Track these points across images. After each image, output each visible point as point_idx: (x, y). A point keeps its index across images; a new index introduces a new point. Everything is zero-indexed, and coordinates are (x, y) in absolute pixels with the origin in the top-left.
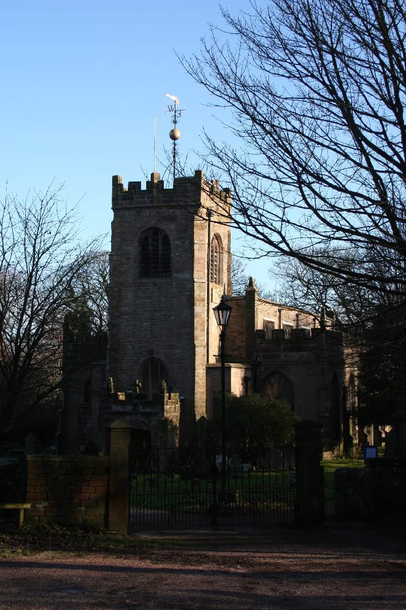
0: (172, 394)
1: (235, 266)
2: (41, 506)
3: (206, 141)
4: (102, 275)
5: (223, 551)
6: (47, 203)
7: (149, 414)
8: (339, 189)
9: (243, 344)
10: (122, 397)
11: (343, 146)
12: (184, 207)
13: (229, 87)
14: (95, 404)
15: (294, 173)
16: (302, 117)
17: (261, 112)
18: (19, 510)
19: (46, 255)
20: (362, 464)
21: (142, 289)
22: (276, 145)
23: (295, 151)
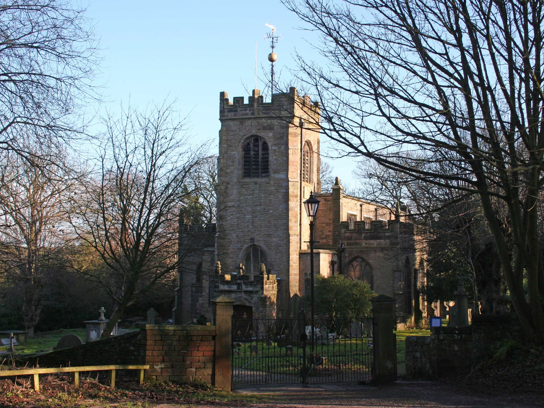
0: (270, 276)
1: (324, 169)
2: (158, 367)
3: (297, 58)
4: (212, 176)
5: (310, 404)
6: (164, 113)
7: (251, 292)
8: (409, 101)
9: (330, 234)
10: (228, 277)
11: (412, 64)
12: (281, 118)
13: (316, 15)
14: (206, 284)
15: (371, 87)
16: (377, 40)
17: (343, 36)
18: (139, 371)
19: (162, 157)
20: (428, 333)
21: (244, 187)
22: (356, 64)
23: (372, 69)
